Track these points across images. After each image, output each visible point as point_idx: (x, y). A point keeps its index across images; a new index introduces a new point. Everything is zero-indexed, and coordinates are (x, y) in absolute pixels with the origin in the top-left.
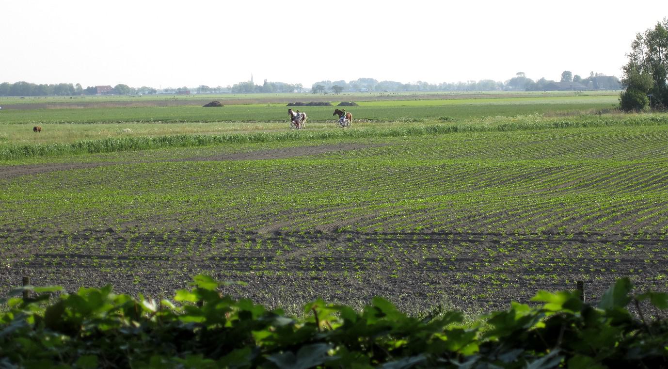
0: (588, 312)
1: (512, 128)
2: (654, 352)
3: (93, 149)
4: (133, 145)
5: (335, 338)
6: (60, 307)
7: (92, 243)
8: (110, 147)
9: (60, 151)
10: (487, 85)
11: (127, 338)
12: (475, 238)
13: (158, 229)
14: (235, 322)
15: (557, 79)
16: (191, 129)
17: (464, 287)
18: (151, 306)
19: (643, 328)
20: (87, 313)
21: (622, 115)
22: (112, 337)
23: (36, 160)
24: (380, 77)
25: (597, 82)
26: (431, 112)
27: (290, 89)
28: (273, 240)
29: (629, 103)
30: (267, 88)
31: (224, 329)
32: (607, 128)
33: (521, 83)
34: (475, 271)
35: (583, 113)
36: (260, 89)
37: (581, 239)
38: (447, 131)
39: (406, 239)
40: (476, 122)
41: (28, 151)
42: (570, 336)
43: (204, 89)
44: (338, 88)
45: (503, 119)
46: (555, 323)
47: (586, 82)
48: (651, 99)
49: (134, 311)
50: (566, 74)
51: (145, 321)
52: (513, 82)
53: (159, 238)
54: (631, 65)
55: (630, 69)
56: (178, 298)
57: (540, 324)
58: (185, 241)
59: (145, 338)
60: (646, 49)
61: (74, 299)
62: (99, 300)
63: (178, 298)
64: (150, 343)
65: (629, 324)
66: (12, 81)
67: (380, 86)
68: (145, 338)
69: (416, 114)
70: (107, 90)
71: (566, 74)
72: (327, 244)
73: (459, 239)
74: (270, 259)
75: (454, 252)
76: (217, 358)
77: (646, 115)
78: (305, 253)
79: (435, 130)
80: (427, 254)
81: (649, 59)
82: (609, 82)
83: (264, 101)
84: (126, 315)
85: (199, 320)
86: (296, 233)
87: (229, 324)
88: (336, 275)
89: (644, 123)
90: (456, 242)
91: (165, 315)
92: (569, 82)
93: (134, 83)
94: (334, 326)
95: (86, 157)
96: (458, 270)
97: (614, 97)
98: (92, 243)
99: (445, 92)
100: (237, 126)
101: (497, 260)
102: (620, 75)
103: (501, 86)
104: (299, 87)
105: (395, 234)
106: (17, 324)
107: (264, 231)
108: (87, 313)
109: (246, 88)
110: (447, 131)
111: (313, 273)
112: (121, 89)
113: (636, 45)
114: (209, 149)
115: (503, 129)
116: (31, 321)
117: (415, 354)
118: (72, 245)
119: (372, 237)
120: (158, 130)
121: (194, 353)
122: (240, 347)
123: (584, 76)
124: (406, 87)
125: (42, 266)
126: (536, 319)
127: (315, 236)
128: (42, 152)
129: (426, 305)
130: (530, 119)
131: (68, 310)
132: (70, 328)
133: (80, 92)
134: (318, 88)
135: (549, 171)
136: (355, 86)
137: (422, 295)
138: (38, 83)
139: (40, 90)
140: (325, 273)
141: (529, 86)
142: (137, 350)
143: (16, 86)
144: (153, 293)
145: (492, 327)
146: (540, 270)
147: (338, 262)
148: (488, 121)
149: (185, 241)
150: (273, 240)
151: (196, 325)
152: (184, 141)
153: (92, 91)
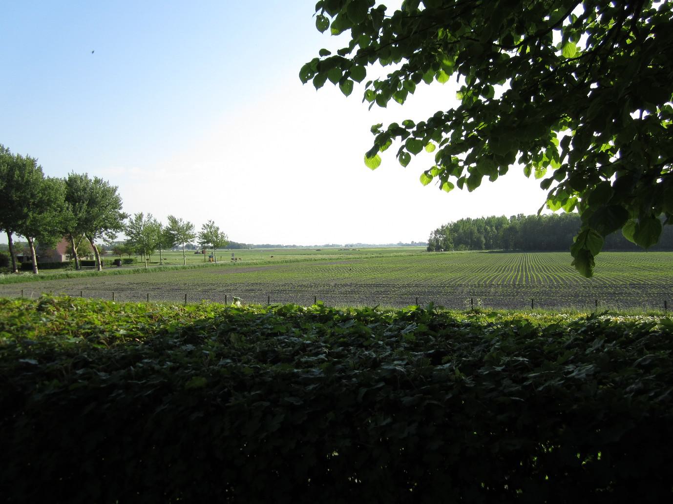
0: (422, 311)
1: (398, 256)
2: (441, 322)
3: (286, 262)
4: (297, 261)
5: (355, 318)
6: (281, 309)
7: (287, 287)
8: (291, 261)
9: (278, 262)
10: (391, 245)
11: (300, 318)
12: (388, 286)
13: (304, 283)
14: (328, 313)
15: (410, 243)
16: (312, 257)
17: (385, 299)
18: (305, 309)
19: (437, 315)
20: (289, 310)
21: (428, 253)
22: (296, 318)
23: (271, 265)
24: (363, 243)
25: (421, 244)
26: (376, 252)
27: (339, 246)
28: (335, 286)
29: (429, 250)
30: (333, 245)
31: (325, 315)
32: (424, 256)
33: (400, 244)
34: (388, 294)
35: (417, 252)
36: (331, 246)
37: (417, 286)
38: (381, 257)
39: (370, 286)
40: (388, 255)
41: (269, 262)
42: (418, 318)
43: (316, 246)
44: (351, 246)
45: (395, 254)
46: (414, 314)
47: (418, 244)
48: (436, 249)
49: (301, 310)
50: (412, 242)
51: (304, 313)
52: (398, 244)
53: (304, 286)
54: (430, 239)
55: (430, 240)
56: (312, 306)
57: (409, 314)
58: (311, 287)
59: (304, 318)
60: (434, 235)
61: (285, 307)
62: (292, 307)
63: (312, 306)
64: (305, 319)
65: (433, 314)
66: (265, 244)
67: (363, 245)
68: (304, 318)
69: (372, 252)
70: (290, 246)
71: (412, 242)
72: (349, 287)
73: (384, 286)
74: (334, 291)
75: (383, 289)
76: (324, 323)
77: (434, 253)
78: (343, 290)
79: (378, 257)
80: (375, 290)
81: (435, 238)
82: (424, 244)
83: (332, 249)
84: (299, 311)
85: (318, 313)
86: (341, 284)
87: (326, 314)
88: (351, 296)
89: (434, 255)
90: (383, 287)
91: (309, 311)
92: (413, 244)
93: (298, 245)
94: (355, 314)
95: (285, 264)
96: (384, 294)
97: (425, 248)
98: (287, 287)
99: (381, 247)
100: (325, 256)
101: (394, 291)
102: (427, 242)
103: (395, 245)
104: (341, 245)
105: (367, 284)
106: (270, 314)
107: (332, 284)
108: (289, 310)
109: (327, 246)
110: (381, 257)
111: (345, 295)
112: (294, 246)
113: (431, 234)
114: (318, 262)
115: (396, 256)
116: (273, 313)
117: (376, 322)
118: (281, 288)
119: (361, 286)
120: (304, 257)
121: (318, 322)
122: (330, 320)
123: (417, 242)
124: (370, 245)
125: (273, 293)
126: (408, 313)
127: (346, 285)
128: (273, 263)
129: (376, 304)
130: (402, 254)
131: (283, 310)
132: (284, 315)
133: (283, 247)
134: (346, 246)
135: (408, 268)
136: (356, 245)
137: (374, 301)
138: (272, 244)
139: (273, 246)
140: (348, 295)
141: (403, 245)
142: (302, 321)
143: (266, 245)
144: (305, 306)
145: (397, 315)
146: (406, 294)
147: (352, 292)
148: (392, 255)
149: (311, 287)
150: (335, 286)
151: (318, 314)
152: (311, 260)
153: (286, 246)
